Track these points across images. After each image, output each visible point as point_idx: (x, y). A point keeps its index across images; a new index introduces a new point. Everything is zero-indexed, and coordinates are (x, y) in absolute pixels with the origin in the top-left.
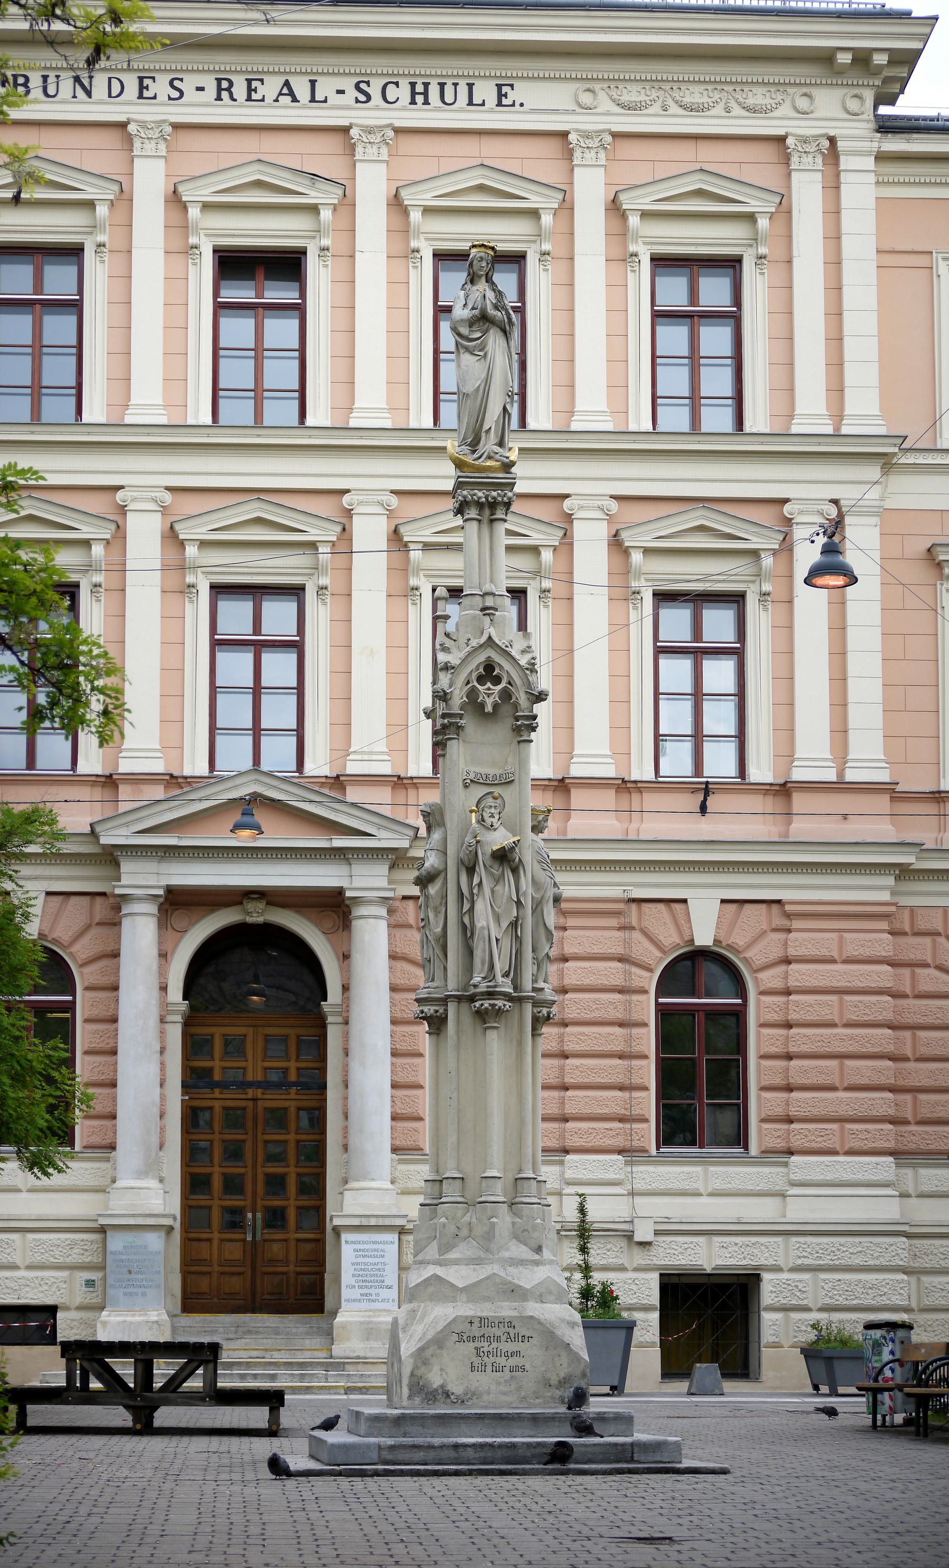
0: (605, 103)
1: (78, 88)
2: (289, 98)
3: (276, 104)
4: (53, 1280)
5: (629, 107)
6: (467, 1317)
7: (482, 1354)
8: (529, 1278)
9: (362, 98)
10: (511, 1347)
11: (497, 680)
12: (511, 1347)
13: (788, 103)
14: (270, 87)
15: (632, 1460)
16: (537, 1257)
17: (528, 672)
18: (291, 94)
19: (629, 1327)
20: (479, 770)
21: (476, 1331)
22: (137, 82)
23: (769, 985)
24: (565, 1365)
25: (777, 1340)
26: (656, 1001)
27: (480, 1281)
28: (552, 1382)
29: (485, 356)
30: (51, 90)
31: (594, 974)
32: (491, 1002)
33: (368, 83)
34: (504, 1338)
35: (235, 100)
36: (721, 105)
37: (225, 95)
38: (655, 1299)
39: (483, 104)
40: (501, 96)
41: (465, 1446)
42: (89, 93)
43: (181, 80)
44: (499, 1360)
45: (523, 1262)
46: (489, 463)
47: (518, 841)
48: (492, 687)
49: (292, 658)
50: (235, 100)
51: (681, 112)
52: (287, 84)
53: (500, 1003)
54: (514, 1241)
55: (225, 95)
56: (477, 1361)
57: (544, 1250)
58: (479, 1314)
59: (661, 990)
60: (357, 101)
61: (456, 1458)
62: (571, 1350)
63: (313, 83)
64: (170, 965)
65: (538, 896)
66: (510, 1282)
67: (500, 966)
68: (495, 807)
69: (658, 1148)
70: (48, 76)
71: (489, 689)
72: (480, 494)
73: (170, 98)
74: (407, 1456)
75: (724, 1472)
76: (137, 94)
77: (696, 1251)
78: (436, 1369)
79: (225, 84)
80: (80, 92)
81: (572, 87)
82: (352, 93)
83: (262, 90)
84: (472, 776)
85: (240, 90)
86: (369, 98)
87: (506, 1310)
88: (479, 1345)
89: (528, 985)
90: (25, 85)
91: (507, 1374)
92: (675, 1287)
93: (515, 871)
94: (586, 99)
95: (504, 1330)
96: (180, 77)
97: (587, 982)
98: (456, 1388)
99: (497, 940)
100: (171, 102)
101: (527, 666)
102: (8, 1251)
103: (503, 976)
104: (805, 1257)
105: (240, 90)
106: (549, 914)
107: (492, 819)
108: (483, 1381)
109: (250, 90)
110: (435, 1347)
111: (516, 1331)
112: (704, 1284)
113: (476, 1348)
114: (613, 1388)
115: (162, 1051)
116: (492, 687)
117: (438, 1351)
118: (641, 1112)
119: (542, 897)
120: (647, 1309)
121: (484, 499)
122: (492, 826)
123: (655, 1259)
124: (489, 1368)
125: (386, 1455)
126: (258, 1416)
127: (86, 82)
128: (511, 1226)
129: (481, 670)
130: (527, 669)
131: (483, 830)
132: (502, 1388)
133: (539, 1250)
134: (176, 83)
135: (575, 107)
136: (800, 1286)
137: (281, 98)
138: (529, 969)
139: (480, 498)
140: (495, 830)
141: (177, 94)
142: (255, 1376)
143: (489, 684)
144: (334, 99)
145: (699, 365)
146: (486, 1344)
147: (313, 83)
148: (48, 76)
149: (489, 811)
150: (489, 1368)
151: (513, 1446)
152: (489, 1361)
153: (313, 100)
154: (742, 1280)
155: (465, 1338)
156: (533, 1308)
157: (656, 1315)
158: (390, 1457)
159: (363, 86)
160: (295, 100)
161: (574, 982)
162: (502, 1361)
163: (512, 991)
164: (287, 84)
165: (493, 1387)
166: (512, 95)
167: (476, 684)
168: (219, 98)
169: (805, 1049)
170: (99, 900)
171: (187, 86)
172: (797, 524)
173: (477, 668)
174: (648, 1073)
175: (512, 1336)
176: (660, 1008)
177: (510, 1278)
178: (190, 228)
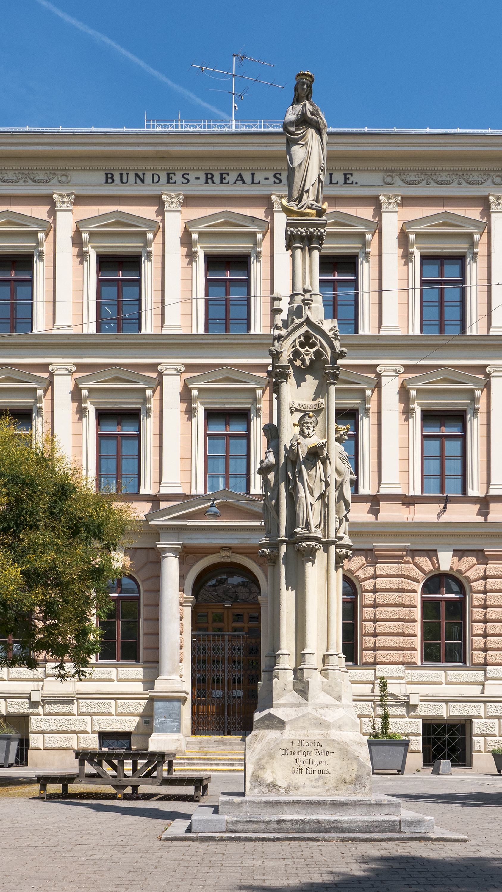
0: (398, 181)
1: (138, 179)
2: (241, 182)
3: (235, 185)
4: (130, 720)
5: (409, 183)
6: (290, 740)
7: (300, 763)
8: (331, 716)
9: (277, 181)
10: (319, 758)
11: (312, 345)
12: (319, 758)
13: (490, 180)
14: (232, 177)
15: (400, 832)
16: (337, 703)
17: (333, 339)
18: (242, 180)
19: (406, 744)
20: (300, 402)
21: (296, 748)
22: (166, 175)
23: (477, 588)
24: (356, 770)
25: (479, 749)
26: (421, 596)
27: (299, 718)
28: (347, 780)
29: (306, 144)
30: (125, 180)
31: (391, 583)
32: (308, 543)
33: (280, 174)
34: (314, 753)
35: (215, 183)
36: (456, 182)
37: (210, 181)
38: (420, 731)
39: (337, 183)
40: (346, 179)
41: (285, 821)
42: (143, 181)
43: (188, 174)
44: (311, 766)
45: (328, 707)
46: (308, 211)
47: (326, 442)
48: (309, 349)
49: (245, 442)
50: (215, 183)
51: (436, 185)
52: (240, 175)
53: (313, 544)
54: (323, 693)
55: (210, 181)
56: (296, 767)
57: (343, 698)
58: (298, 738)
59: (424, 591)
60: (275, 183)
61: (279, 829)
62: (359, 761)
63: (253, 175)
64: (185, 580)
65: (339, 479)
66: (319, 718)
67: (314, 521)
68: (311, 423)
69: (421, 663)
70: (123, 174)
71: (307, 351)
72: (302, 230)
73: (182, 183)
74: (245, 827)
75: (464, 841)
76: (166, 181)
77: (440, 709)
78: (269, 771)
79: (209, 176)
80: (138, 181)
81: (380, 175)
82: (272, 179)
83: (228, 179)
84: (296, 406)
85: (217, 179)
86: (280, 181)
87: (315, 734)
88: (296, 756)
89: (332, 535)
90: (112, 178)
91: (316, 774)
92: (429, 725)
93: (324, 463)
94: (389, 180)
95: (314, 748)
96: (188, 173)
97: (387, 587)
98: (282, 783)
99: (312, 505)
100: (183, 185)
101: (333, 336)
102: (108, 707)
103: (315, 528)
104: (493, 712)
105: (217, 179)
106: (347, 491)
107: (308, 430)
108: (301, 779)
109: (222, 178)
110: (268, 758)
111: (322, 748)
112: (443, 725)
113: (296, 759)
114: (399, 771)
115: (181, 618)
116: (309, 349)
117: (270, 761)
118: (413, 646)
119: (343, 480)
120: (417, 735)
121: (304, 234)
122: (308, 434)
123: (420, 712)
124: (304, 771)
125: (231, 827)
126: (189, 790)
127: (142, 176)
128: (320, 683)
129: (302, 338)
130: (332, 337)
131: (301, 437)
132: (313, 783)
133: (339, 698)
134: (186, 176)
135: (383, 184)
136: (491, 725)
137: (237, 182)
138: (333, 524)
139: (302, 233)
140: (310, 437)
141: (186, 181)
142: (223, 764)
143: (307, 348)
144: (263, 182)
145: (444, 306)
146: (302, 756)
147: (253, 175)
148: (123, 174)
149: (306, 425)
150: (304, 771)
151: (318, 822)
152: (304, 767)
153: (253, 182)
154: (463, 722)
155: (288, 752)
156: (334, 734)
157: (420, 738)
158: (233, 828)
159: (278, 176)
160: (244, 183)
161: (381, 587)
162: (313, 767)
163: (321, 536)
164: (240, 175)
165: (307, 783)
166: (352, 179)
167: (298, 347)
168: (207, 182)
169: (494, 617)
170: (150, 551)
171: (191, 177)
172: (493, 376)
173: (299, 337)
174: (418, 628)
175: (320, 752)
176: (423, 599)
177: (319, 716)
178: (193, 244)
